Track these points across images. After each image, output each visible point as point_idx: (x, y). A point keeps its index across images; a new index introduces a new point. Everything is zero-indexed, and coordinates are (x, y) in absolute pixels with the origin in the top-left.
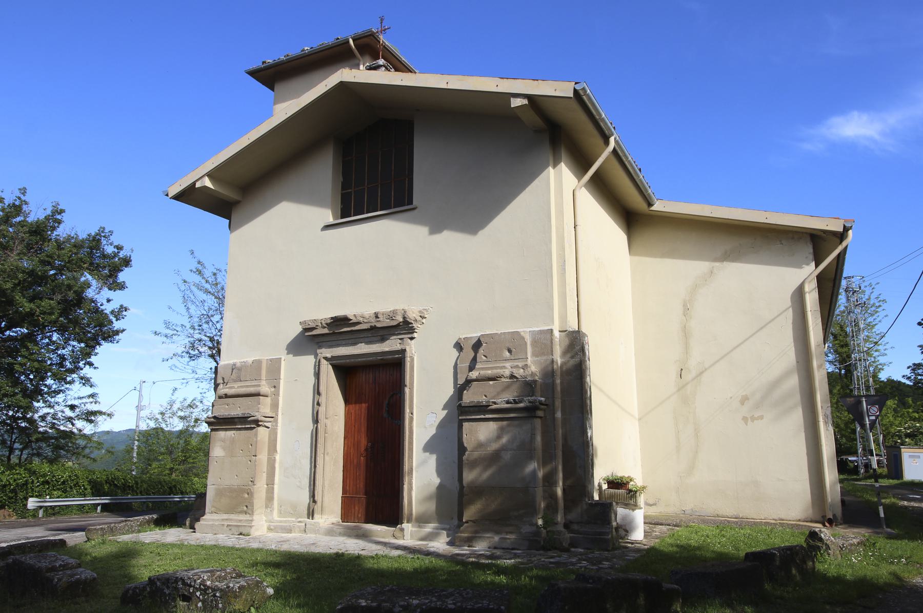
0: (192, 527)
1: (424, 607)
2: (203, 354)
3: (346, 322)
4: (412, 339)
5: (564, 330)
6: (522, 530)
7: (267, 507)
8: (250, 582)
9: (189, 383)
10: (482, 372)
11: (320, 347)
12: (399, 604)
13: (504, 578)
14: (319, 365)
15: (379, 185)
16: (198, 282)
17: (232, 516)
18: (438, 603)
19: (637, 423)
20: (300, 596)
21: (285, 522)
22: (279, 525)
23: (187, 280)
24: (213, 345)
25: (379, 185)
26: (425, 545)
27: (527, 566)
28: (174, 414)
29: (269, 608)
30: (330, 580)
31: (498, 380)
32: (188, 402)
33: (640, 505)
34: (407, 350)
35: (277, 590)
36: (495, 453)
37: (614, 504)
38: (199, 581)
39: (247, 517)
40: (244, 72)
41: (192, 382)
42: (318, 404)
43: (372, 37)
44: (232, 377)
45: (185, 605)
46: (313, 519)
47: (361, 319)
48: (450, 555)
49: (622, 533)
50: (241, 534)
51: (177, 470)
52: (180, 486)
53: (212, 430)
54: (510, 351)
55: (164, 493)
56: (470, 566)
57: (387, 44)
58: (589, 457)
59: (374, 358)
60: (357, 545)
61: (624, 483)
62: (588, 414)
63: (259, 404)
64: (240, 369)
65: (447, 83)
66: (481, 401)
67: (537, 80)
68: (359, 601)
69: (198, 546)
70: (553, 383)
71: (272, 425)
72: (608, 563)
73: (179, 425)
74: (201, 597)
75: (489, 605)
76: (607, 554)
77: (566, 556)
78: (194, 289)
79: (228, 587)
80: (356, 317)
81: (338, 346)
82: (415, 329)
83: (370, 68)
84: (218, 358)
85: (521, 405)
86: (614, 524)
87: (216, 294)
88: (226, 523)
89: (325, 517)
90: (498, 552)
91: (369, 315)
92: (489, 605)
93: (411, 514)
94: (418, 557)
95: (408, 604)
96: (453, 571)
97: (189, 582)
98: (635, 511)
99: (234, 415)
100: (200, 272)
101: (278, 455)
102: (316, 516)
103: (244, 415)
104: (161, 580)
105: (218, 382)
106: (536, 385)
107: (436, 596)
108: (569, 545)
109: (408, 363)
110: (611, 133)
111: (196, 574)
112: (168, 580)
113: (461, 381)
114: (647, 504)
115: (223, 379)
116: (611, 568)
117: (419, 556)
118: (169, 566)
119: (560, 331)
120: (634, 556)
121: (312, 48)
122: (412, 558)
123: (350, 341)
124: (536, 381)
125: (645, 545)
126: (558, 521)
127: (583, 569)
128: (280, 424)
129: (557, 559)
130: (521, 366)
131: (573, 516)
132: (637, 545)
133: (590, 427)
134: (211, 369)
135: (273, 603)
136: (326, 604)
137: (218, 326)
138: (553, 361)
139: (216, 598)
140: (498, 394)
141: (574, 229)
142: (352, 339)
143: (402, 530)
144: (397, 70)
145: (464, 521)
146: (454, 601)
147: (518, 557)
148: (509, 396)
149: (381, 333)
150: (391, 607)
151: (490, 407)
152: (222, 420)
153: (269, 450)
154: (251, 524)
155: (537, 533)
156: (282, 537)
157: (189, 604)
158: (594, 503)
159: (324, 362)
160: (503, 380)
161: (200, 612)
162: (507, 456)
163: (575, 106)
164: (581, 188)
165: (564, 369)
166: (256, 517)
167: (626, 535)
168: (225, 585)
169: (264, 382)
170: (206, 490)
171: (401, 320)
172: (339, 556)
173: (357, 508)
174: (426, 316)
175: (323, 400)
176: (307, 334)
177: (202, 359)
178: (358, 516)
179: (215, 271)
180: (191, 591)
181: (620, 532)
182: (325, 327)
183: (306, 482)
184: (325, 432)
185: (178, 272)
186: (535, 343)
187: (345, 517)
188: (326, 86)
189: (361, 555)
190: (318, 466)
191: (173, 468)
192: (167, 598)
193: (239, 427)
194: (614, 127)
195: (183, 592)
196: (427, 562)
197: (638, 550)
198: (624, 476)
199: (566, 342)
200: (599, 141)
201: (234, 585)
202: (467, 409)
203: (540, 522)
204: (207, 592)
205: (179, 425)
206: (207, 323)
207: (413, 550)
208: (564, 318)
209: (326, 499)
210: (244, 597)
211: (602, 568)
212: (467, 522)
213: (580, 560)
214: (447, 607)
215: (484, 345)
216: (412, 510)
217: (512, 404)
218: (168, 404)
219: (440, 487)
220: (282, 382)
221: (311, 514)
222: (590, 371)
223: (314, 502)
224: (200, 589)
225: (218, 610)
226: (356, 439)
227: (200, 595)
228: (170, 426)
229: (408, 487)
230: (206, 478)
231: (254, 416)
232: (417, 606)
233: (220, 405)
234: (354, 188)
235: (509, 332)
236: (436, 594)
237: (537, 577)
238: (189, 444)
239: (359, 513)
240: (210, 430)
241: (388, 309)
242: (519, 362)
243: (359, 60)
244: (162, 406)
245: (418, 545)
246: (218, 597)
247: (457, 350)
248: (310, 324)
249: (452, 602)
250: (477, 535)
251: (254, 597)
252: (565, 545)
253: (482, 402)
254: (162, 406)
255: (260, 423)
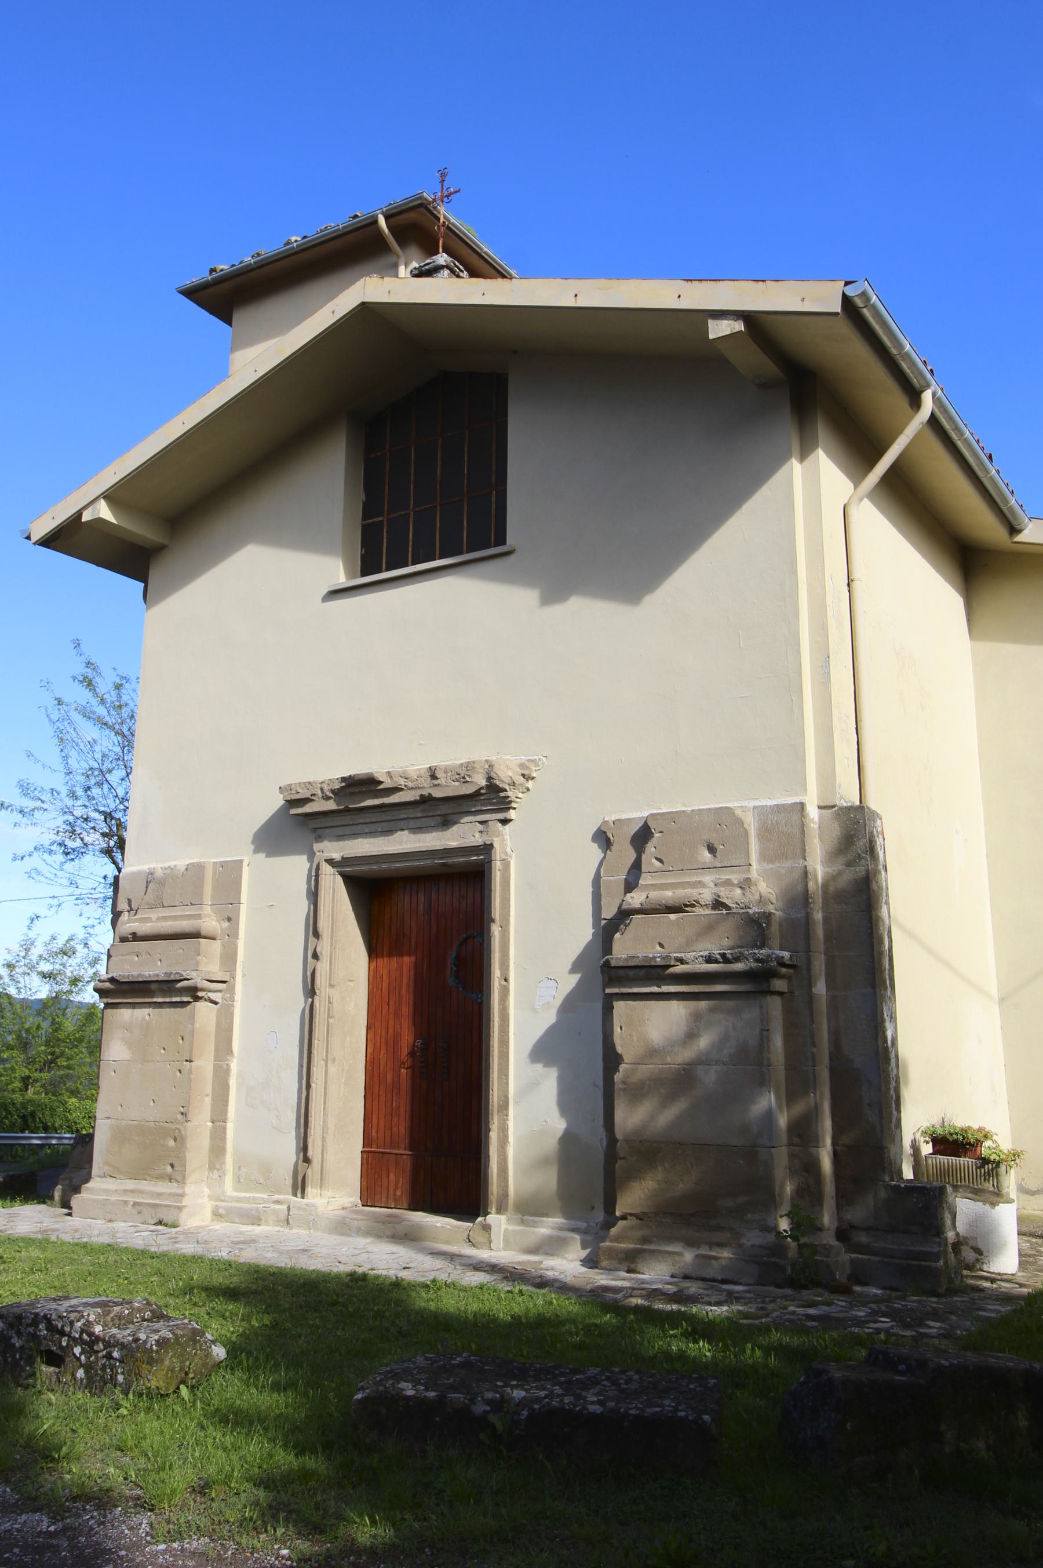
0: (66, 1204)
1: (536, 1406)
2: (90, 847)
3: (372, 787)
4: (505, 822)
5: (829, 804)
6: (744, 1241)
7: (212, 1168)
8: (179, 1332)
9: (63, 906)
10: (656, 895)
11: (319, 838)
12: (482, 1397)
13: (707, 1346)
14: (317, 876)
15: (438, 507)
16: (84, 704)
17: (145, 1185)
18: (567, 1400)
19: (996, 1009)
20: (279, 1364)
21: (248, 1200)
22: (236, 1207)
23: (65, 699)
24: (111, 830)
25: (438, 507)
26: (535, 1262)
27: (757, 1322)
28: (32, 967)
29: (217, 1386)
30: (339, 1333)
31: (688, 912)
32: (60, 942)
33: (1008, 1194)
34: (495, 845)
35: (234, 1350)
36: (684, 1069)
37: (949, 1189)
38: (79, 1324)
39: (172, 1188)
40: (175, 291)
41: (69, 904)
42: (315, 956)
43: (422, 210)
44: (146, 898)
45: (51, 1374)
46: (303, 1198)
47: (402, 782)
48: (589, 1287)
49: (969, 1255)
50: (160, 1223)
51: (36, 1081)
52: (43, 1114)
53: (108, 1005)
54: (712, 849)
55: (11, 1128)
56: (632, 1317)
57: (452, 221)
58: (889, 1083)
59: (429, 862)
60: (394, 1256)
61: (969, 1144)
62: (886, 989)
63: (199, 955)
64: (161, 883)
65: (576, 295)
66: (651, 956)
67: (764, 281)
68: (400, 1386)
69: (77, 1244)
70: (807, 922)
71: (223, 998)
72: (938, 1324)
73: (41, 988)
74: (83, 1357)
75: (676, 1409)
76: (936, 1303)
77: (843, 1304)
78: (76, 717)
79: (136, 1340)
80: (391, 778)
81: (355, 835)
82: (511, 802)
83: (420, 273)
84: (118, 856)
85: (739, 966)
86: (950, 1235)
87: (117, 727)
88: (131, 1199)
89: (327, 1193)
90: (693, 1288)
91: (418, 773)
92: (676, 1409)
93: (505, 1195)
94: (521, 1291)
95: (502, 1396)
96: (596, 1325)
97: (60, 1326)
98: (996, 1207)
99: (150, 975)
100: (89, 683)
101: (235, 1060)
102: (309, 1190)
103: (169, 976)
104: (6, 1318)
105: (119, 909)
106: (769, 923)
107: (560, 1384)
108: (849, 1278)
109: (498, 873)
110: (923, 384)
111: (73, 1309)
112: (19, 1318)
113: (609, 912)
114: (1022, 1190)
115: (130, 901)
116: (946, 1335)
117: (524, 1288)
118: (19, 1284)
119: (820, 807)
120: (999, 1312)
121: (305, 237)
122: (508, 1292)
123: (379, 827)
124: (770, 914)
125: (1021, 1285)
126: (823, 1225)
127: (882, 1336)
128: (238, 997)
129: (823, 1310)
130: (736, 882)
131: (859, 1213)
132: (1003, 1284)
133: (891, 1017)
134: (105, 877)
135: (224, 1376)
136: (333, 1385)
137: (121, 792)
138: (805, 873)
139: (112, 1361)
140: (688, 944)
141: (846, 588)
142: (382, 822)
143: (487, 1228)
144: (474, 274)
145: (618, 1214)
146: (601, 1398)
147: (738, 1299)
148: (714, 945)
149: (444, 809)
150: (466, 1401)
151: (671, 970)
152: (125, 987)
153: (217, 1051)
154: (181, 1203)
155: (778, 1248)
156: (241, 1233)
157: (60, 1372)
158: (902, 1185)
159: (327, 870)
160: (698, 911)
161: (80, 1388)
162: (709, 1077)
163: (845, 329)
164: (861, 500)
165: (831, 889)
166: (189, 1189)
167: (978, 1260)
168: (129, 1335)
169: (207, 910)
170: (94, 1131)
171: (483, 783)
172: (357, 1280)
173: (392, 1176)
174: (534, 775)
175: (324, 947)
176: (293, 811)
177: (88, 858)
178: (395, 1194)
179: (118, 680)
180: (64, 1344)
181: (964, 1254)
182: (330, 798)
183: (290, 1118)
184: (329, 1013)
185: (46, 685)
186: (766, 832)
187: (370, 1194)
188: (333, 312)
189: (403, 1280)
190: (313, 1085)
191: (29, 1077)
192: (18, 1356)
193: (160, 1000)
194: (931, 370)
195: (49, 1346)
196: (540, 1302)
197: (1007, 1298)
198: (969, 1127)
199: (835, 831)
200: (899, 400)
201: (148, 1337)
202: (621, 972)
203: (784, 1225)
204: (95, 1348)
205: (41, 988)
206: (100, 784)
207: (511, 1273)
208: (827, 778)
209: (330, 1157)
210: (167, 1362)
211: (925, 1335)
212: (624, 1217)
213: (874, 1313)
214: (587, 1409)
215: (657, 835)
216: (507, 1186)
217: (720, 963)
218: (22, 946)
219: (567, 1140)
220: (243, 909)
221: (300, 1186)
222: (887, 895)
223: (307, 1160)
224: (80, 1341)
225: (115, 1387)
226: (391, 1030)
227: (81, 1354)
228: (26, 992)
229: (499, 1135)
230: (94, 1099)
231: (187, 979)
232: (522, 1403)
233: (122, 955)
234: (388, 514)
235: (710, 809)
236: (563, 1379)
237: (781, 1350)
238: (59, 1029)
239: (396, 1188)
240: (102, 1006)
241: (455, 759)
242: (732, 872)
243: (398, 257)
244: (9, 951)
245: (519, 1263)
246: (116, 1359)
247: (599, 847)
248: (300, 790)
249: (595, 1399)
250: (645, 1247)
251: (187, 1363)
252: (841, 1276)
253: (655, 958)
254: (9, 951)
255: (200, 994)
